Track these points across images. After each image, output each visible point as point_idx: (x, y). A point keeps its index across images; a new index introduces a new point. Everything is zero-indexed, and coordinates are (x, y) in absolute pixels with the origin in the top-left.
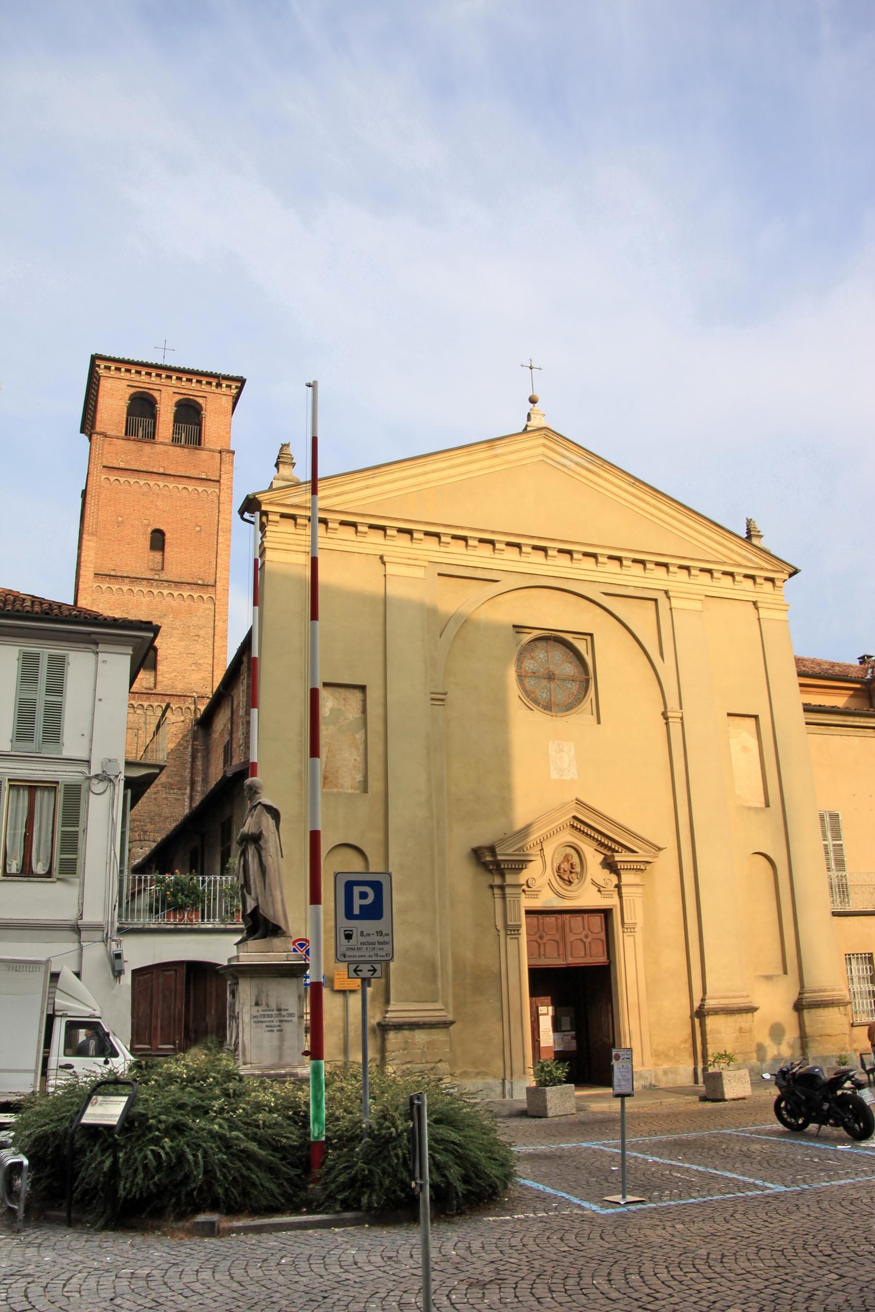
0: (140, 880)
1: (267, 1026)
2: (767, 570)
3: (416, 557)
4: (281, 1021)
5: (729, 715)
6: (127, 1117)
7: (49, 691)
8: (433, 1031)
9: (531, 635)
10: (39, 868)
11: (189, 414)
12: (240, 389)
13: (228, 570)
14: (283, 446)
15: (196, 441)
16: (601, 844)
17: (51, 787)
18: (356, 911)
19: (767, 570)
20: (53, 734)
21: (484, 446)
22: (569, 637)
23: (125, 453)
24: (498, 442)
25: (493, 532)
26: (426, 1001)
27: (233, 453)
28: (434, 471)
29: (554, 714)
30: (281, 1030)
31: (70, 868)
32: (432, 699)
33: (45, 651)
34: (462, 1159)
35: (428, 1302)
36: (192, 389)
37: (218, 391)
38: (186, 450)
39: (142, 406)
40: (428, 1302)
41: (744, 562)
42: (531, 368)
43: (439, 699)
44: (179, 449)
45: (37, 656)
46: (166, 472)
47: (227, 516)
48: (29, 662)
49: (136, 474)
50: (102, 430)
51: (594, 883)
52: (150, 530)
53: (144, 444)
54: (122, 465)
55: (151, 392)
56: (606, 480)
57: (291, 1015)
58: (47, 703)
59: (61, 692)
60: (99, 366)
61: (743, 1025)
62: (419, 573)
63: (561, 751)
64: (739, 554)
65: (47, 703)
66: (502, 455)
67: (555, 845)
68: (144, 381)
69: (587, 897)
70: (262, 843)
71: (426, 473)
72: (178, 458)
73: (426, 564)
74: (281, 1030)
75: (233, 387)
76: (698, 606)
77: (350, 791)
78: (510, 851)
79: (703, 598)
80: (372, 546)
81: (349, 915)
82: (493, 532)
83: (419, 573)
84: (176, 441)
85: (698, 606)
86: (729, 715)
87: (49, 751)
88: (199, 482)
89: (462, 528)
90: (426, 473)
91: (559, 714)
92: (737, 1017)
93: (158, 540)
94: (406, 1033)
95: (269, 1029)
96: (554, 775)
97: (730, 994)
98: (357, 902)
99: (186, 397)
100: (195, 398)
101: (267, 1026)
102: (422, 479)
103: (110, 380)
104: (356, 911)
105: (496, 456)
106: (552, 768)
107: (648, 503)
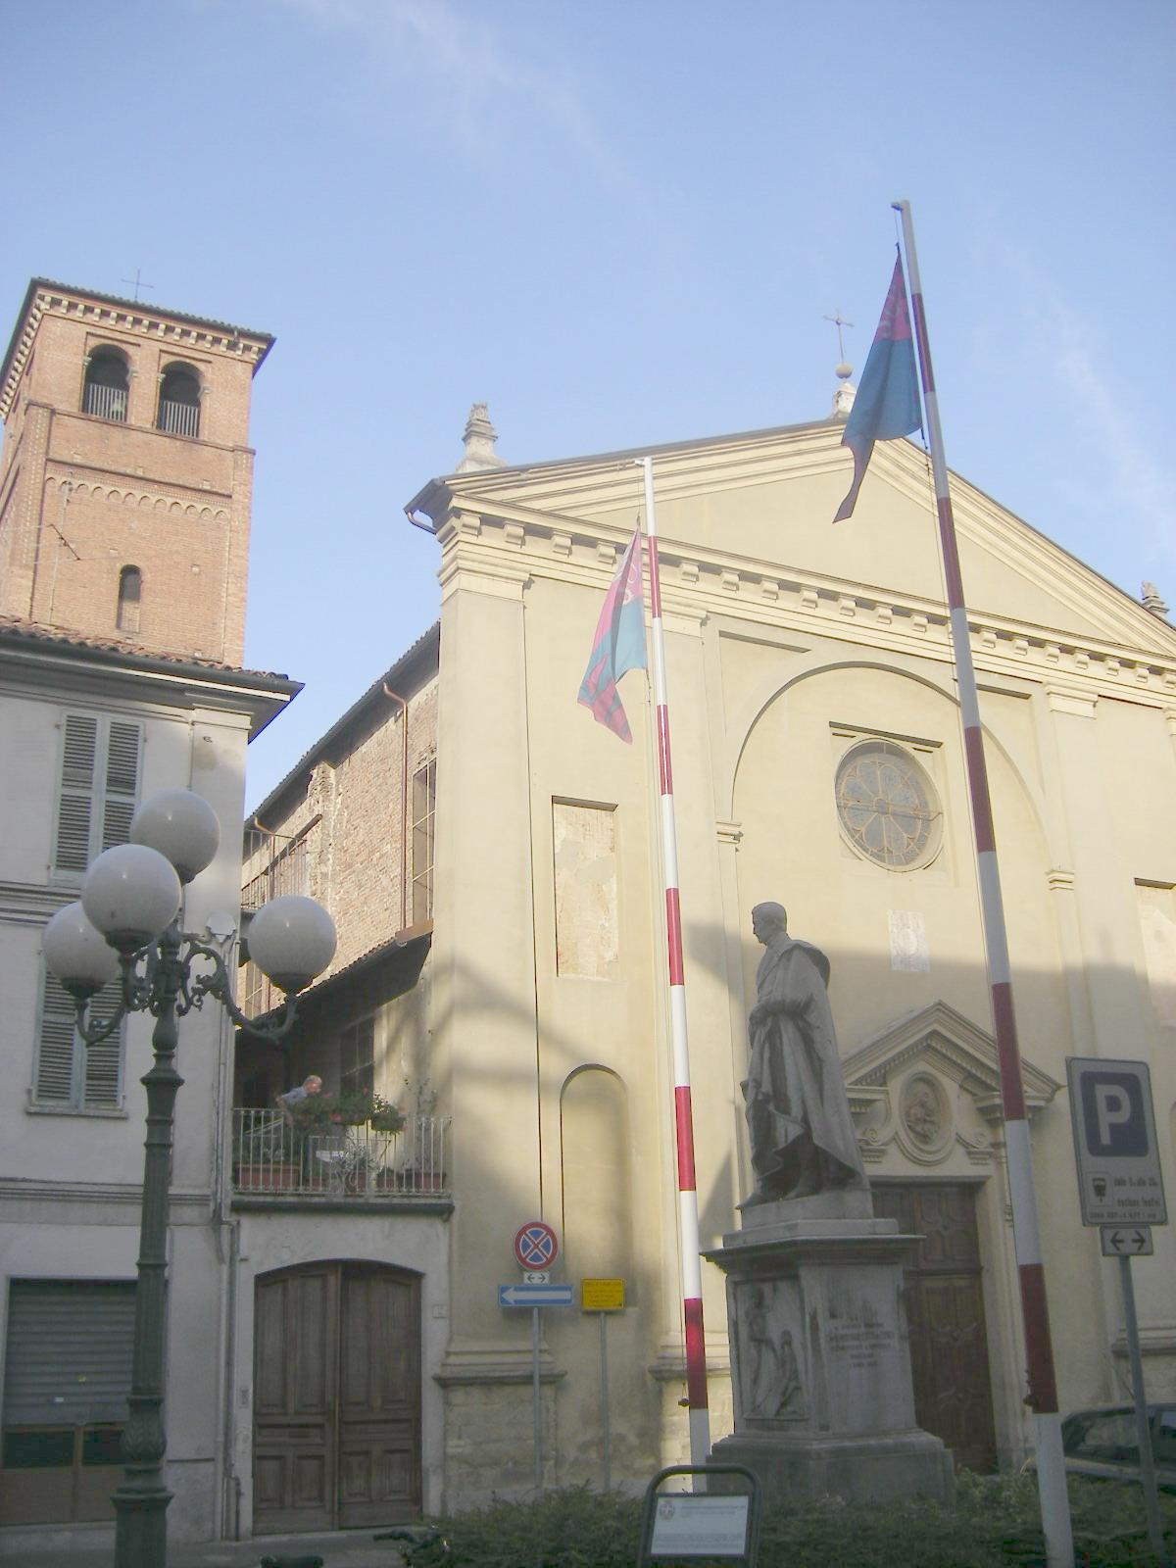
0: (247, 1117)
1: (853, 1357)
3: (690, 602)
4: (874, 1346)
5: (1139, 882)
7: (113, 781)
9: (853, 741)
11: (181, 385)
12: (263, 354)
13: (242, 639)
15: (191, 431)
16: (970, 1076)
18: (1106, 1139)
23: (78, 439)
25: (801, 572)
27: (253, 453)
29: (891, 867)
30: (873, 1364)
36: (189, 347)
37: (231, 354)
38: (178, 443)
39: (107, 368)
44: (167, 440)
45: (91, 726)
46: (147, 476)
47: (241, 553)
48: (79, 737)
49: (99, 475)
50: (45, 401)
51: (960, 1140)
52: (119, 566)
53: (112, 429)
54: (78, 460)
55: (124, 346)
57: (888, 1335)
60: (42, 298)
64: (1142, 635)
65: (109, 805)
68: (113, 329)
69: (957, 1166)
70: (812, 1018)
72: (163, 454)
74: (873, 1364)
75: (255, 349)
77: (596, 978)
79: (1096, 698)
81: (1096, 1148)
82: (801, 572)
84: (160, 423)
85: (1086, 709)
86: (1139, 882)
88: (198, 495)
93: (130, 580)
95: (856, 1361)
97: (1161, 1323)
98: (1106, 1118)
99: (178, 359)
100: (193, 362)
101: (853, 1357)
103: (60, 323)
104: (1106, 1139)
107: (1015, 546)
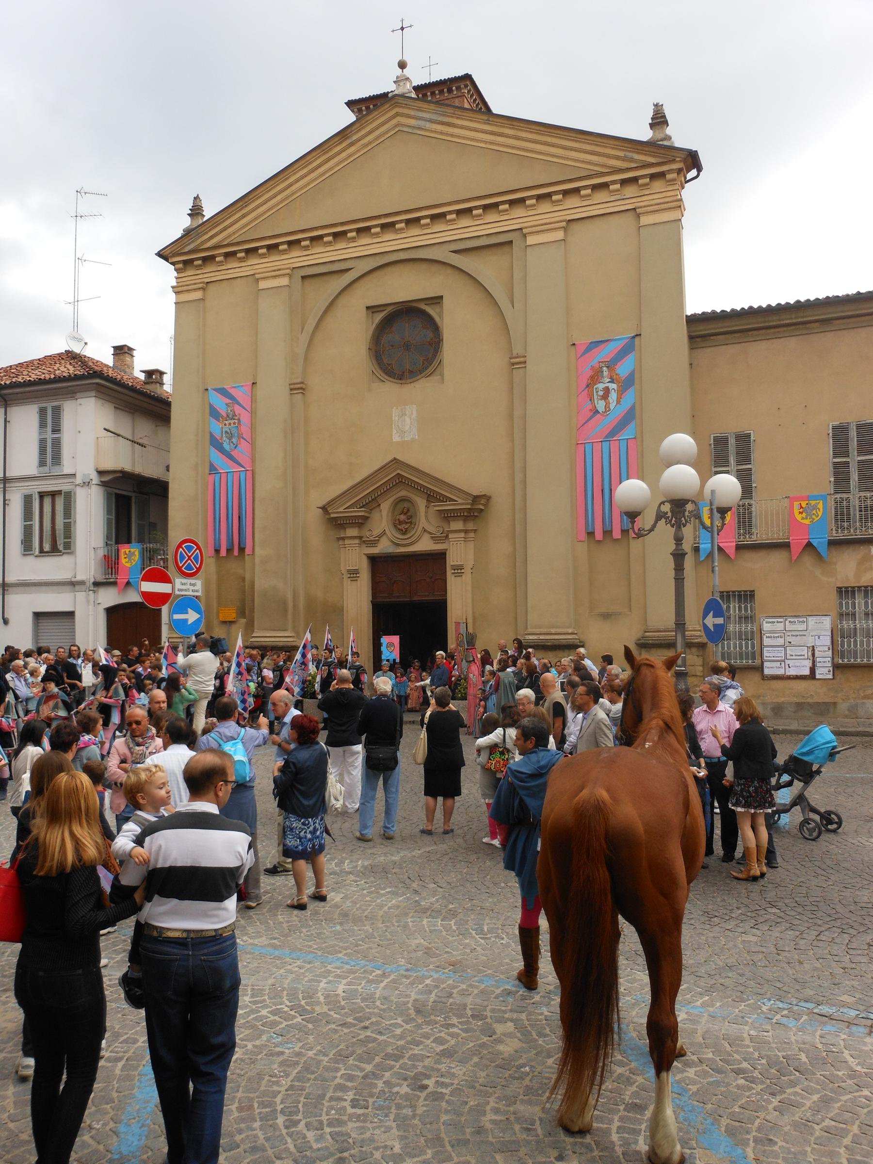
6: (644, 744)
10: (61, 547)
17: (59, 492)
20: (57, 459)
24: (349, 130)
25: (342, 224)
28: (297, 181)
31: (69, 547)
32: (291, 390)
33: (49, 406)
34: (548, 771)
41: (625, 165)
48: (42, 412)
58: (53, 439)
59: (59, 430)
62: (285, 281)
63: (403, 414)
64: (617, 158)
65: (53, 439)
69: (425, 545)
73: (288, 271)
76: (560, 235)
78: (341, 509)
80: (249, 268)
83: (285, 281)
87: (56, 471)
91: (409, 381)
96: (396, 438)
97: (553, 631)
102: (288, 192)
105: (352, 144)
106: (394, 431)
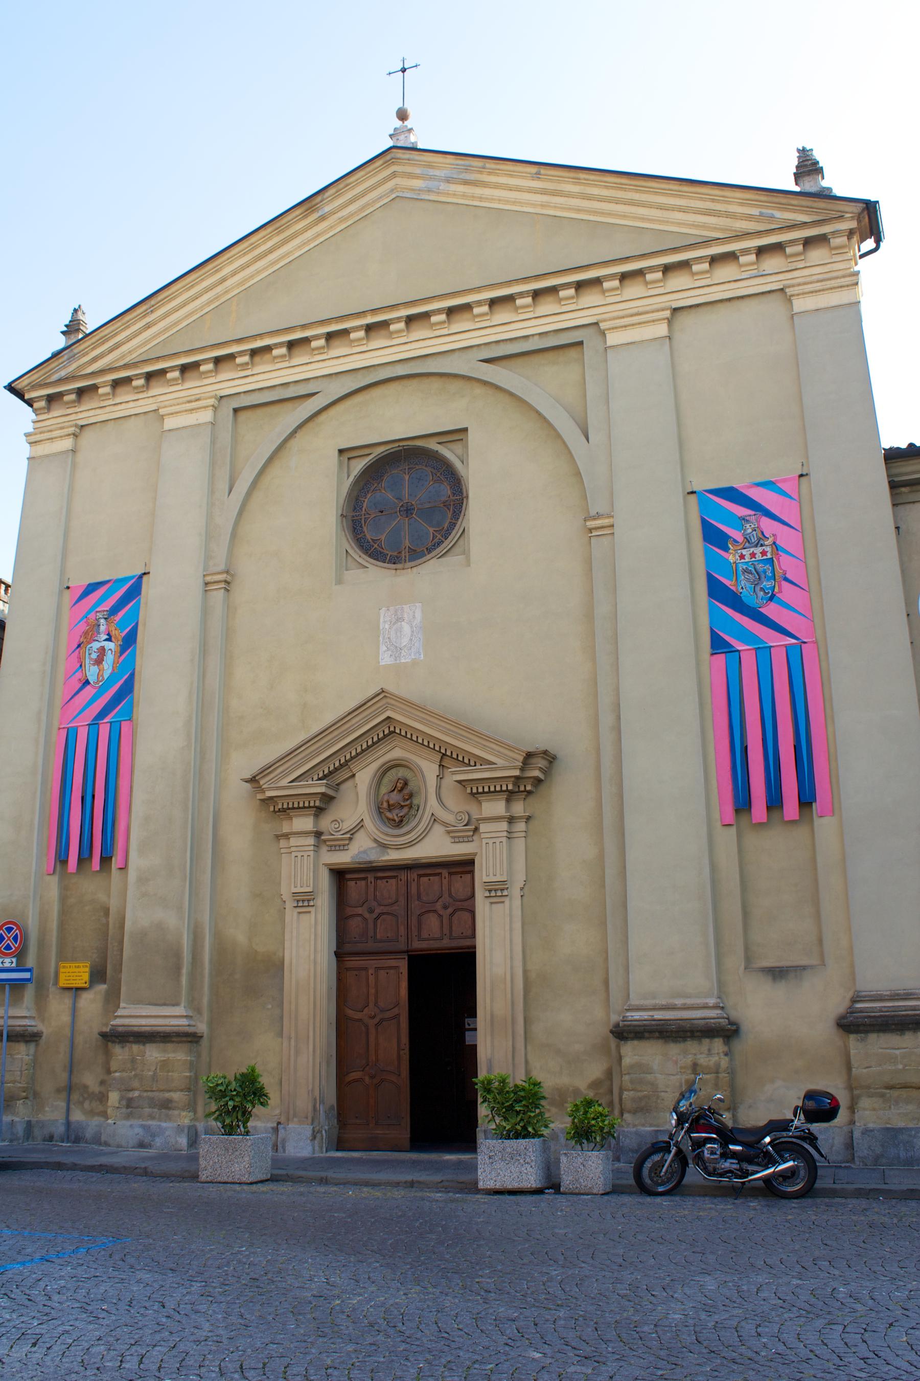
2: (804, 225)
8: (170, 1046)
14: (76, 311)
19: (804, 225)
21: (298, 211)
22: (432, 445)
24: (319, 199)
25: (304, 327)
26: (165, 1004)
35: (911, 1195)
40: (911, 1195)
42: (404, 70)
43: (225, 581)
56: (497, 186)
61: (703, 1060)
63: (399, 619)
66: (332, 213)
67: (375, 766)
71: (223, 280)
89: (260, 336)
90: (223, 280)
92: (692, 1046)
94: (135, 1048)
97: (679, 1002)
105: (323, 218)
